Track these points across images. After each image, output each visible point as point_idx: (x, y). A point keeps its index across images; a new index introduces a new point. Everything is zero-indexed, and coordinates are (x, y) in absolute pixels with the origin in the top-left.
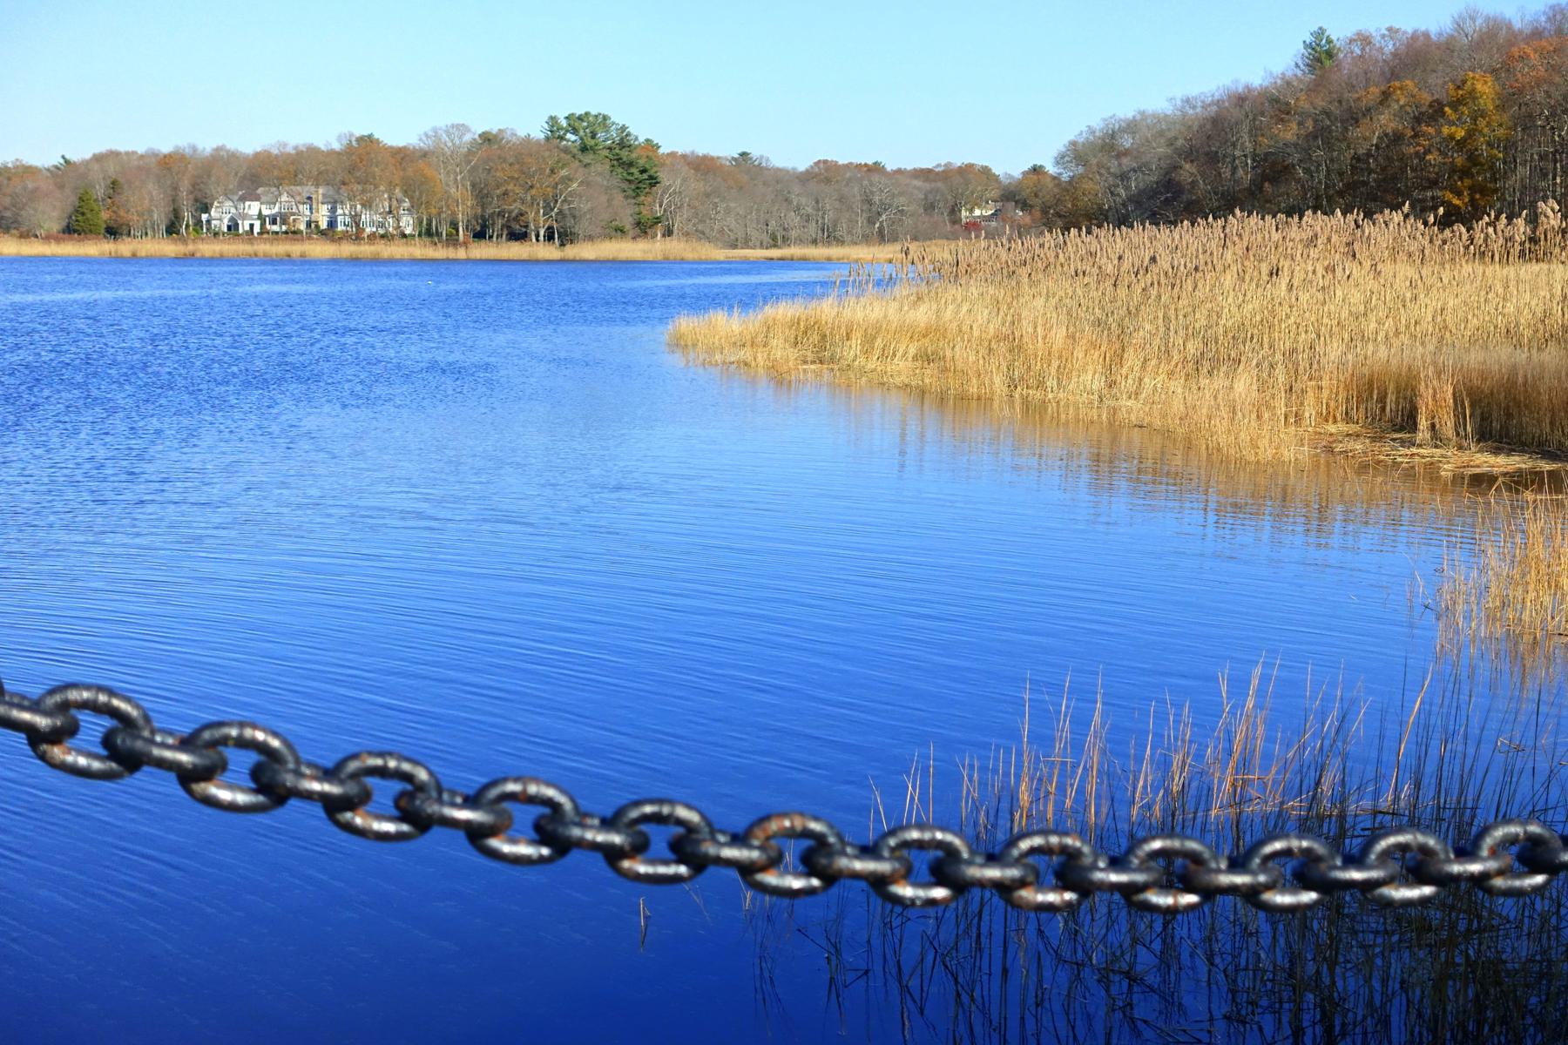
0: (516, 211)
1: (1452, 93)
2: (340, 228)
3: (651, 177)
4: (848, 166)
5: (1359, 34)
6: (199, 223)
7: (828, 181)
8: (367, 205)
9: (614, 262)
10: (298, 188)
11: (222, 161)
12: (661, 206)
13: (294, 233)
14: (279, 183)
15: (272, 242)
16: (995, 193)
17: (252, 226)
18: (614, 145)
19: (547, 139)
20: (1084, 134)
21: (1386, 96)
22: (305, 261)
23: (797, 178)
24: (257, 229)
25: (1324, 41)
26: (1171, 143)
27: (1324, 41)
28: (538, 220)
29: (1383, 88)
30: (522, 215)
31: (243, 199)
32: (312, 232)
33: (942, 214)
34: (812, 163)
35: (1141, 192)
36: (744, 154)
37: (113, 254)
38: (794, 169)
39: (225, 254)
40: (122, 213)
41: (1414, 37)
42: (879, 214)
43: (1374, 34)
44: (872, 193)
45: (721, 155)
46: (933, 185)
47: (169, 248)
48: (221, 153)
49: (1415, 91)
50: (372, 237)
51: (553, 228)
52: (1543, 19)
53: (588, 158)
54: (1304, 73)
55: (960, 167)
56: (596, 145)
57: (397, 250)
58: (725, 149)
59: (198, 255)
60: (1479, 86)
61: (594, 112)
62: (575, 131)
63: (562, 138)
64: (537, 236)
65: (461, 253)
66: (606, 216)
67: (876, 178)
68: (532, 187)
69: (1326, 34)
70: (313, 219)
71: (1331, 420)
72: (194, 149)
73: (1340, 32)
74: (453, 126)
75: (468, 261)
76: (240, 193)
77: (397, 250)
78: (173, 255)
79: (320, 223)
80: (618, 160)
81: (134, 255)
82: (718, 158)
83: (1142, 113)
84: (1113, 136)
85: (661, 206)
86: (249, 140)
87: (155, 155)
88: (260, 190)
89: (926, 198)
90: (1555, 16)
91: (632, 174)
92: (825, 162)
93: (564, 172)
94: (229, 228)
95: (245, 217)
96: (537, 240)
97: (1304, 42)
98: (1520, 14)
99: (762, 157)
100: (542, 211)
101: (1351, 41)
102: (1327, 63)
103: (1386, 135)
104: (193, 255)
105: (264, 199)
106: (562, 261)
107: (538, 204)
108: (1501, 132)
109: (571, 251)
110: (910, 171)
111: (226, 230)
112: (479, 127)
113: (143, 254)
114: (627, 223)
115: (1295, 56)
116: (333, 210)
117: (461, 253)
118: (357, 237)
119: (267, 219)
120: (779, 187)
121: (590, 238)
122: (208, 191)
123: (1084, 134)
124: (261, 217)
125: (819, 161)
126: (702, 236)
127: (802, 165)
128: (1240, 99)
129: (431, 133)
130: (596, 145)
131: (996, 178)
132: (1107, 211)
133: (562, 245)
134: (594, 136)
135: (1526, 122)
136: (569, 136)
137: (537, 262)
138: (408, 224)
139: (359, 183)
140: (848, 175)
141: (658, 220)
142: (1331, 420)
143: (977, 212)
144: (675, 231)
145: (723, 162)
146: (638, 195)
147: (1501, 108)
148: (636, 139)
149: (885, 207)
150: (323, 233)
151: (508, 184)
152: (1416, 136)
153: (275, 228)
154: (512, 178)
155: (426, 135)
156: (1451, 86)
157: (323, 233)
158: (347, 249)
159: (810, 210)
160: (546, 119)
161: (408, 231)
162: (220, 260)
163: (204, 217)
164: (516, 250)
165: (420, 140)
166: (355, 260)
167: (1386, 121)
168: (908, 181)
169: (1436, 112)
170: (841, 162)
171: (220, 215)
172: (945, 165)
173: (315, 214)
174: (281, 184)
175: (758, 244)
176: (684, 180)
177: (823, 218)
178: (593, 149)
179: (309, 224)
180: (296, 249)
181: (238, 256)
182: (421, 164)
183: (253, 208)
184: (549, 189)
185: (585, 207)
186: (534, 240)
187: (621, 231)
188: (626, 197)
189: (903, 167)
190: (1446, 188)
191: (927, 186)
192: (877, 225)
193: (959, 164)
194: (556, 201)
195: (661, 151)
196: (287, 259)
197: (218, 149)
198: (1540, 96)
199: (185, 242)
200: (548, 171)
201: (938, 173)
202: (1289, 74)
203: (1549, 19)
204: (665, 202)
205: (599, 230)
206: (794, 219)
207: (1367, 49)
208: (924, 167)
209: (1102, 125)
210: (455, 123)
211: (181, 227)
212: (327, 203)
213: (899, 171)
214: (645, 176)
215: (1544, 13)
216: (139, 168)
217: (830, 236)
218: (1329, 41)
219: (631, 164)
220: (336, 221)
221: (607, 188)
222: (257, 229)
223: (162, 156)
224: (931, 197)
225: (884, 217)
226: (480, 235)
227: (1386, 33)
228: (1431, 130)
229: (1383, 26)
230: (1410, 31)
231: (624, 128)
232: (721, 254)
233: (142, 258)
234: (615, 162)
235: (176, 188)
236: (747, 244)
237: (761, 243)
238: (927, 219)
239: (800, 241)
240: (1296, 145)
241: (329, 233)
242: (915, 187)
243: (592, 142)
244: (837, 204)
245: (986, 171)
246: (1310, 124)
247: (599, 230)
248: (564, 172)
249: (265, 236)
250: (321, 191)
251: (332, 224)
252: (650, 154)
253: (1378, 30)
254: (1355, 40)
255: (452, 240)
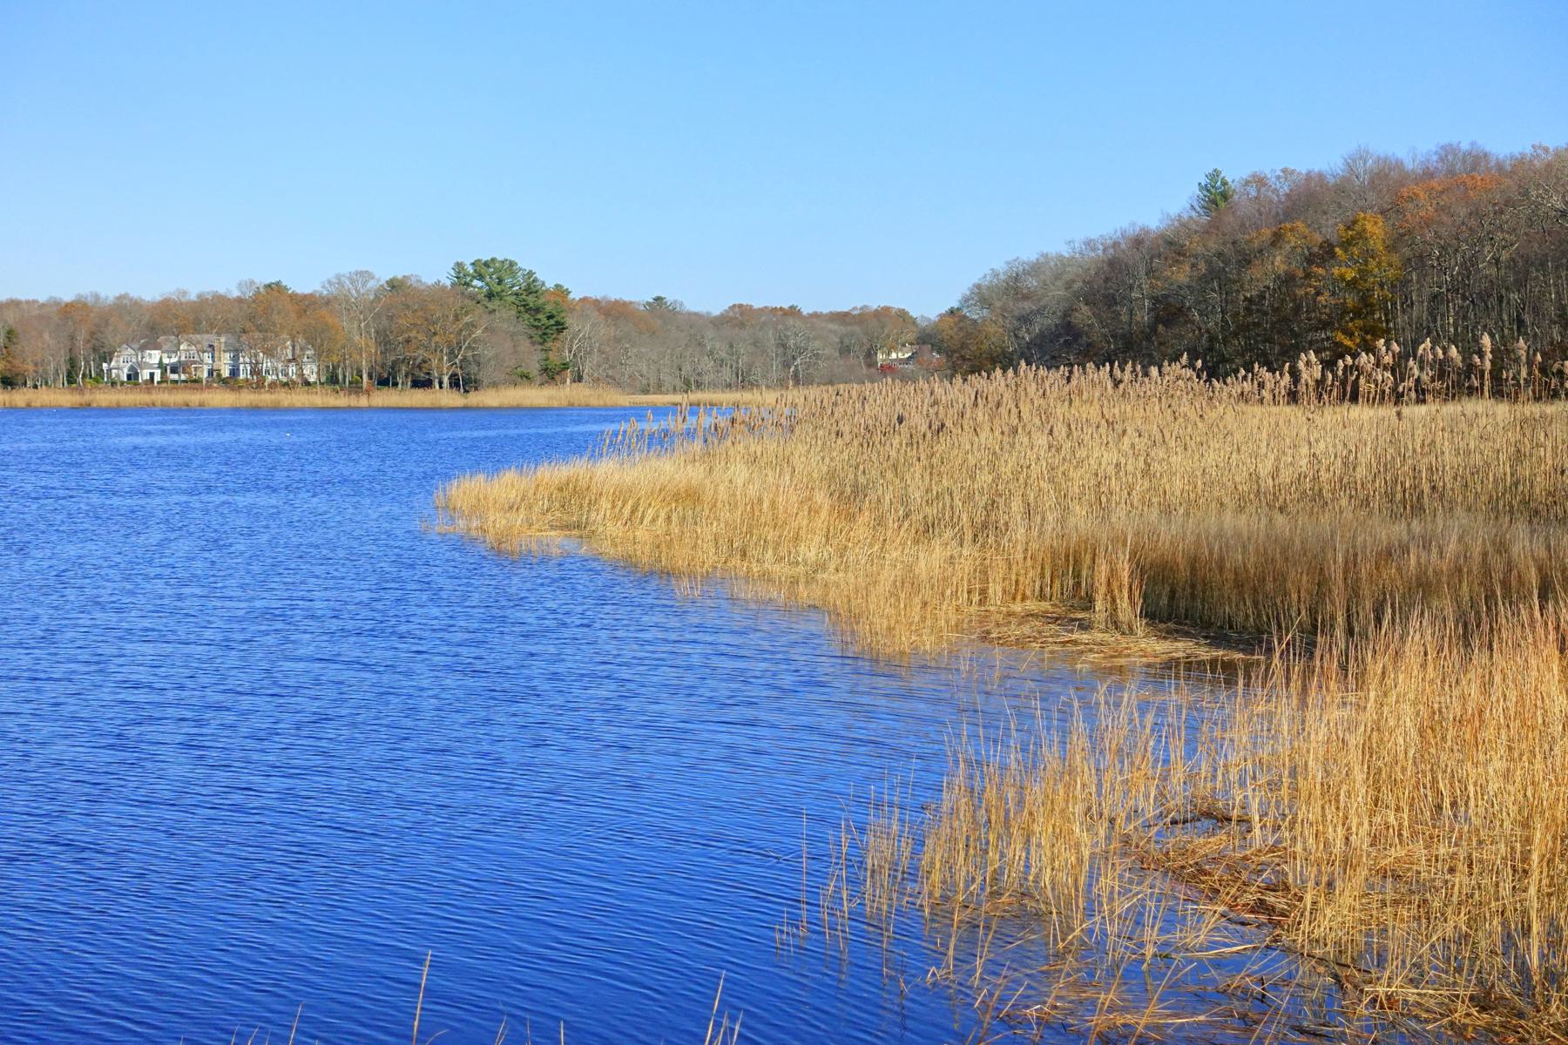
0: (421, 358)
1: (1342, 233)
2: (242, 376)
3: (558, 323)
4: (763, 310)
5: (1254, 176)
6: (100, 373)
7: (742, 325)
8: (270, 353)
9: (518, 408)
10: (198, 336)
11: (125, 308)
12: (570, 352)
13: (195, 381)
14: (180, 331)
15: (170, 391)
16: (911, 336)
17: (152, 375)
18: (521, 292)
19: (453, 285)
20: (988, 278)
21: (1277, 239)
22: (202, 409)
23: (711, 322)
24: (157, 378)
25: (1219, 183)
26: (1069, 285)
27: (1219, 183)
28: (442, 367)
29: (1274, 229)
30: (425, 362)
31: (143, 348)
32: (213, 381)
33: (858, 357)
34: (726, 308)
35: (1042, 335)
36: (658, 299)
37: (7, 405)
38: (709, 313)
39: (122, 404)
40: (17, 362)
41: (1309, 176)
42: (794, 358)
43: (1269, 176)
44: (786, 336)
45: (633, 300)
46: (849, 328)
47: (63, 397)
48: (124, 302)
49: (1302, 236)
50: (273, 385)
51: (457, 375)
52: (1435, 158)
53: (495, 304)
54: (1200, 215)
55: (876, 310)
56: (503, 291)
57: (299, 398)
58: (638, 293)
59: (95, 405)
60: (1369, 227)
61: (500, 258)
62: (481, 277)
63: (467, 284)
64: (441, 383)
65: (363, 401)
66: (513, 363)
67: (790, 321)
68: (435, 334)
69: (1221, 176)
70: (215, 368)
71: (1019, 597)
72: (97, 297)
73: (1234, 174)
74: (357, 273)
75: (370, 408)
76: (142, 341)
77: (299, 398)
78: (69, 405)
79: (222, 372)
80: (524, 306)
81: (29, 405)
82: (631, 303)
83: (1045, 256)
84: (1017, 278)
85: (570, 352)
86: (150, 289)
87: (57, 303)
88: (162, 338)
89: (842, 342)
90: (1446, 156)
91: (539, 320)
92: (740, 306)
93: (468, 319)
94: (129, 377)
95: (142, 365)
96: (441, 387)
97: (1200, 184)
98: (1411, 155)
99: (676, 301)
100: (445, 358)
101: (1247, 183)
102: (1222, 205)
103: (1279, 277)
104: (89, 405)
105: (165, 347)
106: (466, 408)
107: (442, 351)
108: (1391, 273)
109: (475, 398)
110: (826, 315)
111: (125, 379)
112: (383, 275)
113: (38, 405)
114: (534, 368)
115: (1191, 198)
116: (235, 359)
117: (363, 401)
118: (260, 385)
119: (168, 368)
120: (692, 332)
121: (494, 385)
122: (105, 341)
123: (988, 278)
124: (161, 365)
125: (734, 306)
126: (615, 382)
127: (716, 308)
128: (1138, 242)
129: (334, 280)
130: (503, 291)
131: (914, 321)
132: (1012, 354)
133: (466, 391)
134: (500, 282)
135: (1419, 261)
136: (476, 283)
137: (440, 409)
138: (311, 372)
139: (261, 331)
140: (763, 319)
141: (565, 366)
142: (1019, 597)
143: (894, 356)
144: (585, 376)
145: (637, 307)
146: (545, 341)
147: (1391, 248)
148: (543, 284)
149: (801, 351)
150: (225, 381)
151: (411, 331)
152: (1308, 276)
153: (175, 377)
154: (415, 325)
155: (330, 282)
156: (1341, 226)
157: (225, 381)
158: (247, 398)
159: (723, 355)
160: (452, 266)
161: (312, 379)
162: (116, 410)
163: (105, 365)
164: (420, 398)
165: (323, 287)
166: (255, 409)
167: (1279, 263)
168: (824, 324)
169: (1327, 253)
170: (757, 305)
171: (120, 366)
172: (861, 308)
173: (217, 363)
174: (180, 333)
175: (671, 388)
176: (593, 325)
177: (738, 362)
178: (499, 296)
179: (211, 373)
180: (194, 398)
181: (135, 405)
182: (324, 311)
183: (154, 357)
184: (452, 336)
185: (489, 353)
186: (437, 387)
187: (526, 377)
188: (533, 343)
189: (819, 311)
190: (1338, 329)
191: (842, 329)
192: (792, 369)
193: (875, 307)
194: (461, 347)
195: (571, 296)
196: (187, 408)
197: (120, 298)
198: (1429, 236)
199: (81, 391)
200: (451, 318)
201: (854, 316)
202: (1185, 216)
203: (1442, 159)
204: (575, 348)
205: (503, 377)
206: (707, 364)
207: (1263, 189)
208: (839, 309)
209: (1006, 267)
210: (359, 270)
211: (78, 376)
212: (229, 351)
213: (816, 315)
214: (552, 322)
215: (1436, 153)
216: (41, 317)
217: (744, 381)
218: (1225, 183)
219: (538, 310)
220: (238, 369)
221: (513, 335)
222: (157, 378)
223: (63, 304)
224: (846, 341)
225: (799, 361)
226: (385, 382)
227: (1281, 174)
228: (1321, 271)
229: (1278, 168)
230: (1304, 172)
231: (531, 273)
232: (624, 400)
233: (36, 408)
234: (522, 308)
235: (72, 338)
236: (659, 388)
237: (675, 388)
238: (842, 362)
239: (714, 386)
240: (1189, 287)
241: (231, 382)
242: (831, 331)
243: (499, 288)
244: (751, 349)
245: (903, 315)
246: (1203, 267)
247: (503, 377)
248: (468, 319)
249: (164, 385)
250: (223, 339)
251: (234, 372)
252: (560, 300)
253: (1273, 171)
254: (1250, 182)
255: (355, 387)
